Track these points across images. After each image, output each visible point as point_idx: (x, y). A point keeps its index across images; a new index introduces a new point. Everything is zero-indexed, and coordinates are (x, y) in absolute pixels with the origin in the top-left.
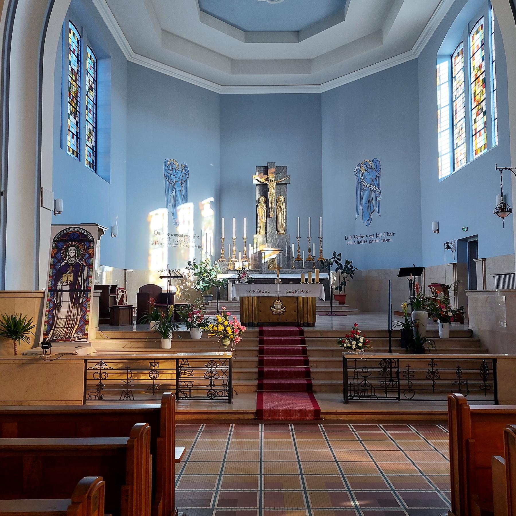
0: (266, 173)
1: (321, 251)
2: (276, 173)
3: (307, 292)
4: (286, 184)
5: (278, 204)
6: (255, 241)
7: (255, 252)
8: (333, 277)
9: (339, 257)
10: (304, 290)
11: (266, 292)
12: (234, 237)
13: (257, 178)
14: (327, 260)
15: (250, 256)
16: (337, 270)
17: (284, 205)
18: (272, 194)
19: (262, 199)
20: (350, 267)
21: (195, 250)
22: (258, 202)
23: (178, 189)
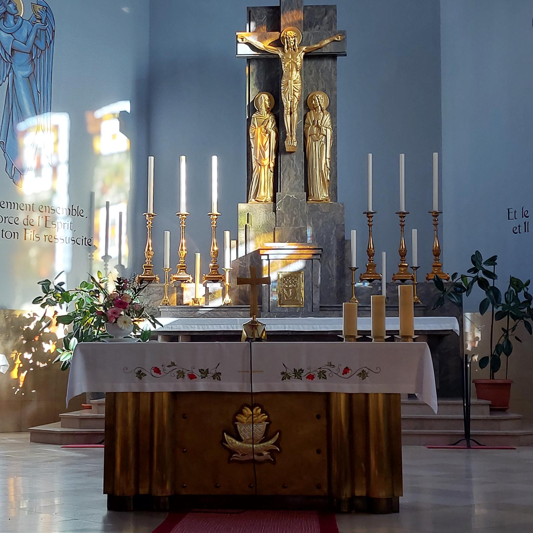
0: (275, 25)
1: (437, 253)
3: (363, 375)
4: (333, 56)
6: (242, 221)
7: (242, 253)
8: (473, 332)
9: (490, 268)
10: (355, 367)
11: (204, 373)
12: (183, 210)
13: (249, 41)
14: (454, 275)
15: (227, 266)
16: (483, 309)
17: (327, 119)
18: (293, 83)
19: (265, 99)
20: (521, 297)
21: (74, 251)
22: (253, 109)
23: (22, 73)
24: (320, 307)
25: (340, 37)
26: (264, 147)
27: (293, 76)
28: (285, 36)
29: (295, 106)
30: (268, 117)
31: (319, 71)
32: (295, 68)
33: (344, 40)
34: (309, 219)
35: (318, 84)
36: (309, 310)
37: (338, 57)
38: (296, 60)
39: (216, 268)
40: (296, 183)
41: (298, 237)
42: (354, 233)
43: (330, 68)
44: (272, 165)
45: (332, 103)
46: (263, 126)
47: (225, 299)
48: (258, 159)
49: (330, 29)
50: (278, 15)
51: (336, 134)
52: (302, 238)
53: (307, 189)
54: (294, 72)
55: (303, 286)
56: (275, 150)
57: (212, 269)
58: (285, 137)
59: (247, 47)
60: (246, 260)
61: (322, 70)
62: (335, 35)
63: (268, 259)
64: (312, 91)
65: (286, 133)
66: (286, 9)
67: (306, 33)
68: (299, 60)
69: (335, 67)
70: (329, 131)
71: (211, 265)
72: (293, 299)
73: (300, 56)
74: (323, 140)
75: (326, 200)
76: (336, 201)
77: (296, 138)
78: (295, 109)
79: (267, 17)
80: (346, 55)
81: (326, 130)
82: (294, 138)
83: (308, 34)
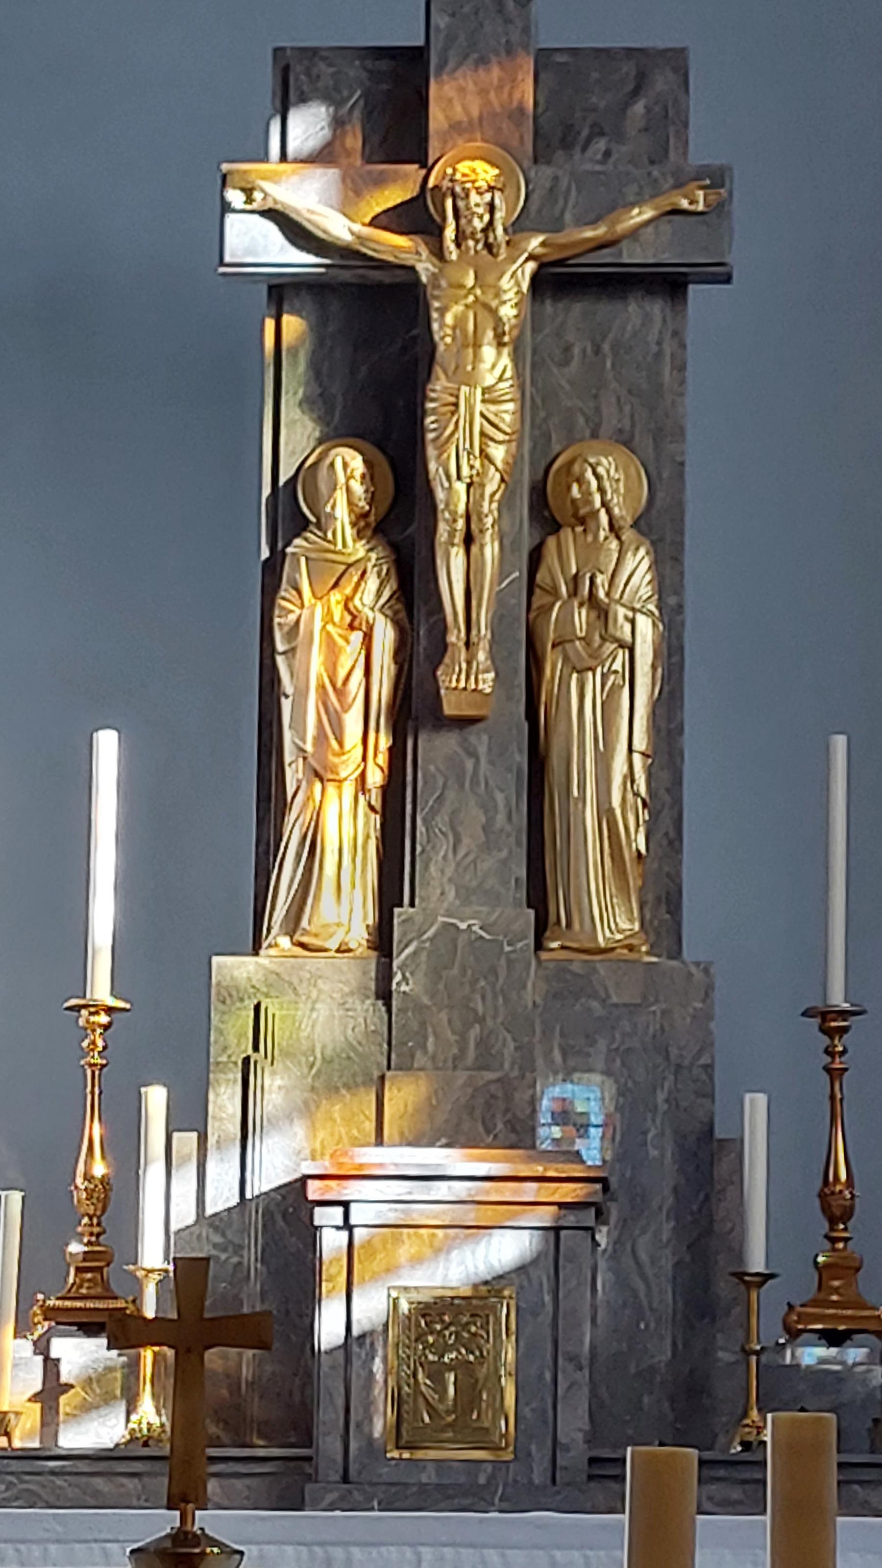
2: (550, 138)
4: (670, 284)
5: (565, 555)
6: (232, 1032)
7: (222, 1195)
13: (295, 196)
15: (153, 1254)
17: (638, 568)
18: (479, 407)
22: (292, 512)
24: (592, 1461)
25: (701, 194)
26: (340, 693)
27: (486, 365)
28: (446, 184)
29: (489, 509)
30: (361, 553)
31: (606, 347)
32: (490, 334)
33: (718, 210)
34: (547, 1032)
35: (598, 410)
36: (539, 1476)
37: (691, 288)
38: (497, 295)
39: (96, 1263)
40: (488, 864)
41: (492, 1115)
42: (756, 1105)
43: (653, 337)
44: (375, 778)
45: (660, 495)
46: (336, 597)
47: (134, 1417)
48: (309, 747)
49: (658, 156)
50: (419, 93)
51: (680, 637)
52: (512, 1126)
53: (538, 894)
54: (488, 352)
55: (511, 1355)
56: (392, 706)
57: (78, 1270)
58: (441, 648)
59: (271, 228)
60: (245, 1230)
61: (616, 347)
62: (679, 185)
63: (347, 1226)
64: (570, 442)
65: (445, 630)
66: (451, 65)
67: (547, 171)
68: (511, 295)
69: (675, 334)
70: (644, 624)
71: (75, 1248)
72: (466, 1419)
73: (515, 280)
74: (618, 666)
75: (631, 948)
76: (676, 953)
77: (492, 655)
78: (489, 521)
79: (365, 95)
80: (727, 279)
81: (633, 622)
82: (482, 656)
83: (556, 179)
